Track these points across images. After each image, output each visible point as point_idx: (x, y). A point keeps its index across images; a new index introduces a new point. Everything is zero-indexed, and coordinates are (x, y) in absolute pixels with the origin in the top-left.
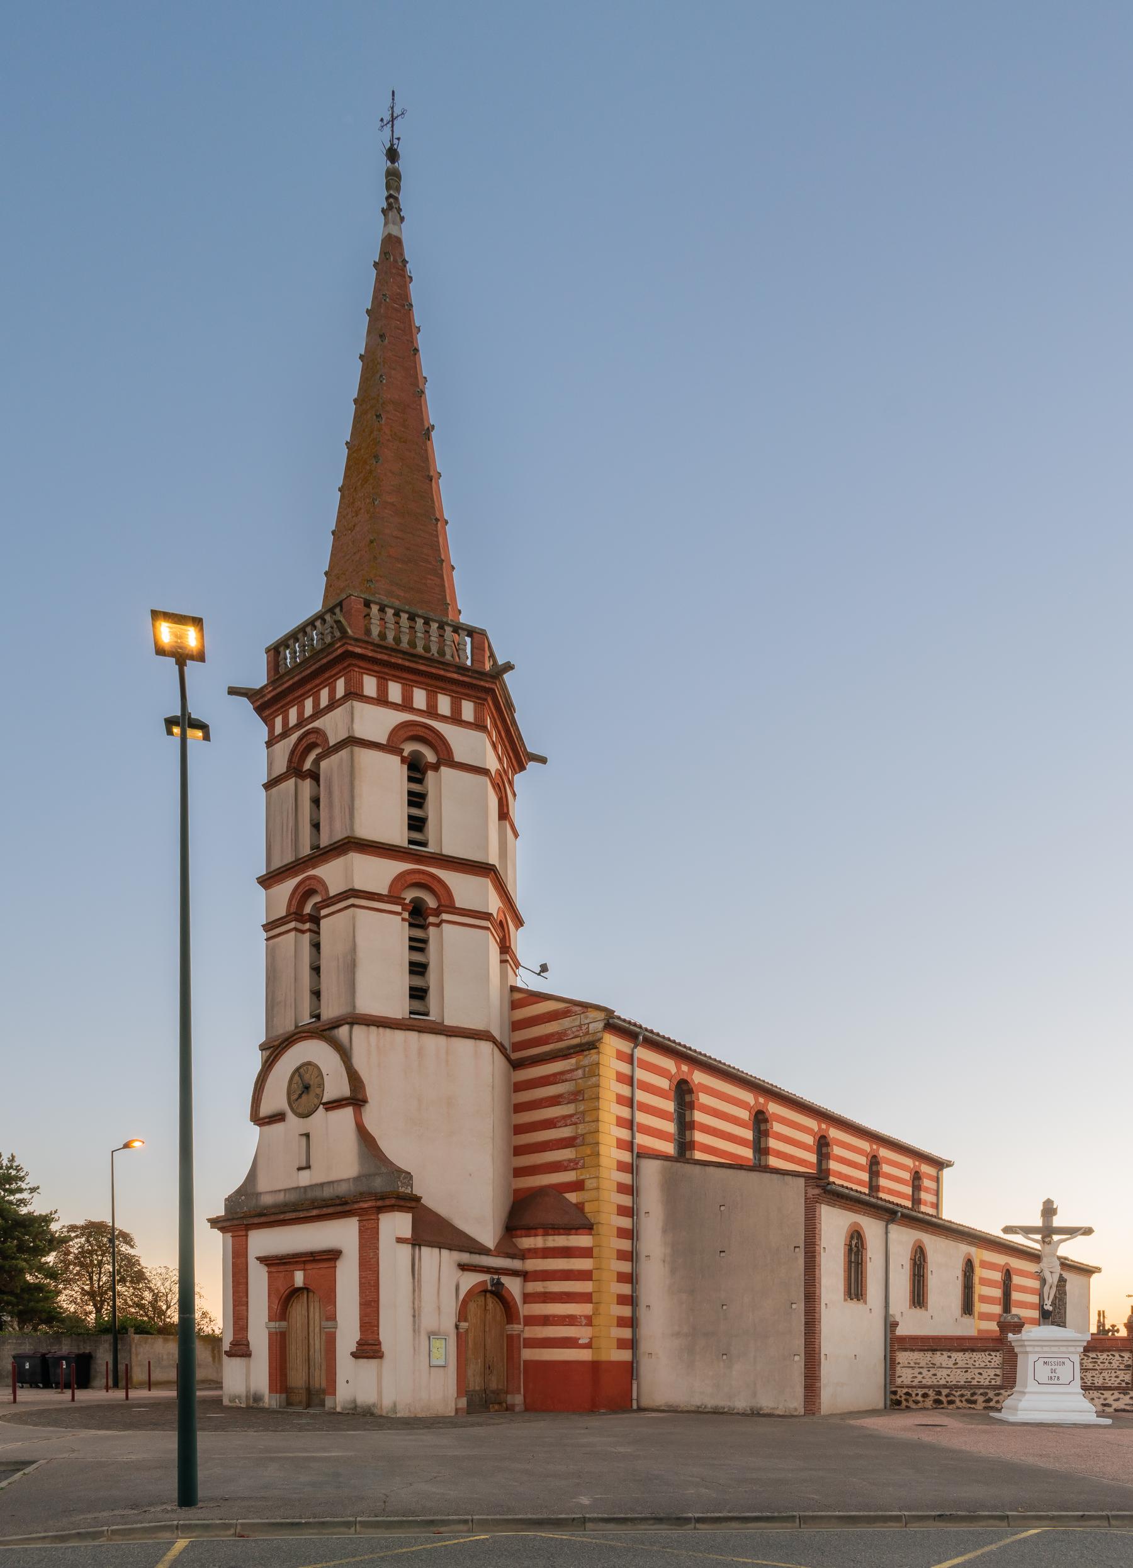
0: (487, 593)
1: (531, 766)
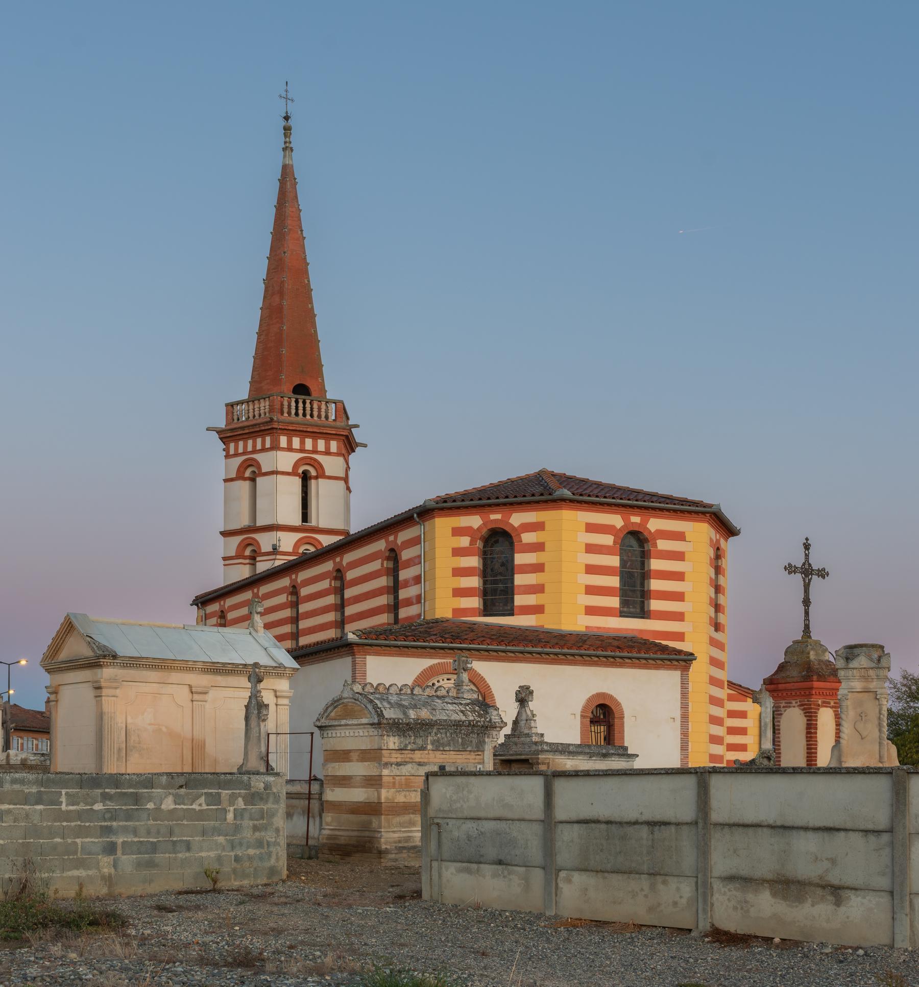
0: (341, 380)
1: (358, 449)
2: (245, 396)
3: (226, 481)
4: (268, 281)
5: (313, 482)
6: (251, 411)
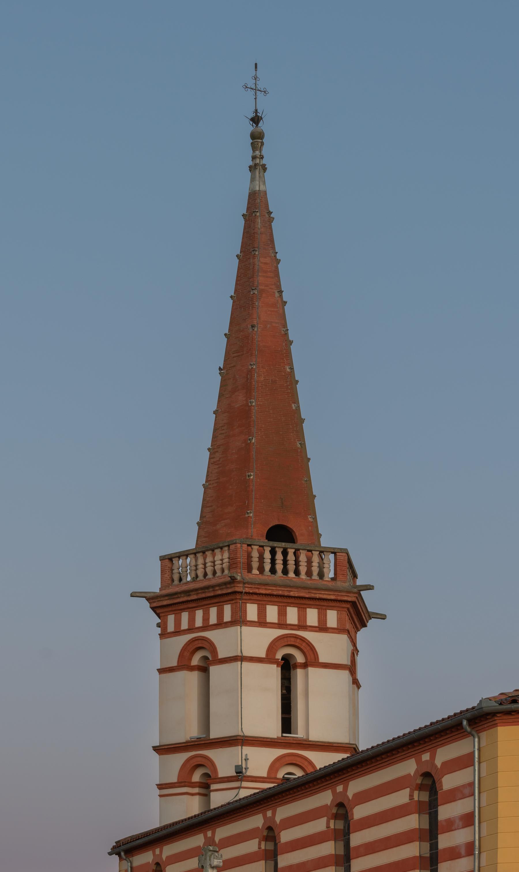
0: (341, 517)
1: (372, 623)
2: (191, 544)
3: (161, 671)
4: (226, 372)
5: (300, 673)
6: (201, 566)
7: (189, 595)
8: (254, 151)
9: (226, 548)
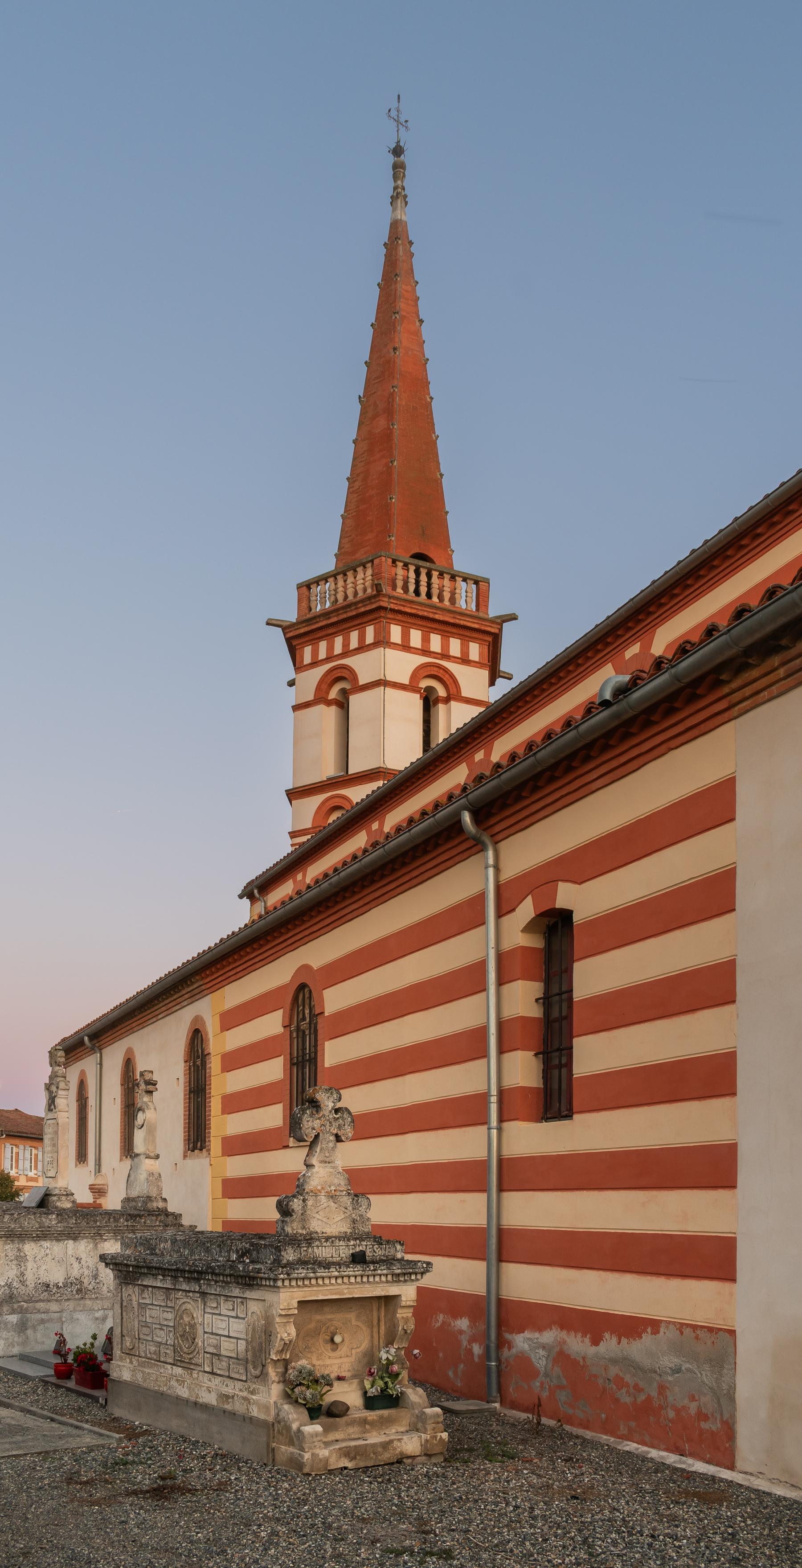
2: (329, 565)
3: (296, 708)
4: (365, 402)
5: (441, 707)
6: (341, 589)
7: (329, 618)
8: (395, 181)
9: (369, 565)
